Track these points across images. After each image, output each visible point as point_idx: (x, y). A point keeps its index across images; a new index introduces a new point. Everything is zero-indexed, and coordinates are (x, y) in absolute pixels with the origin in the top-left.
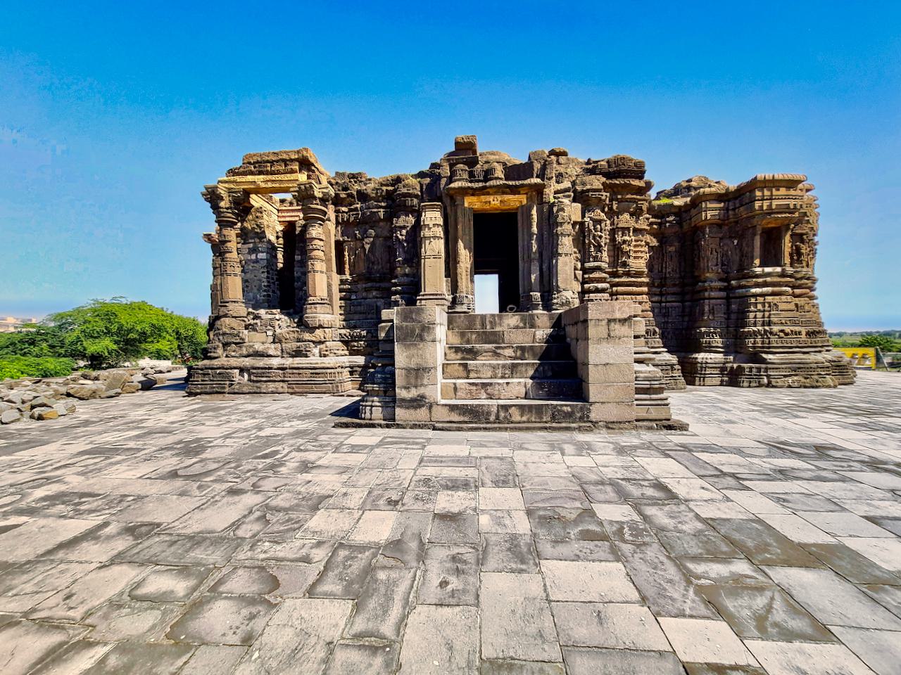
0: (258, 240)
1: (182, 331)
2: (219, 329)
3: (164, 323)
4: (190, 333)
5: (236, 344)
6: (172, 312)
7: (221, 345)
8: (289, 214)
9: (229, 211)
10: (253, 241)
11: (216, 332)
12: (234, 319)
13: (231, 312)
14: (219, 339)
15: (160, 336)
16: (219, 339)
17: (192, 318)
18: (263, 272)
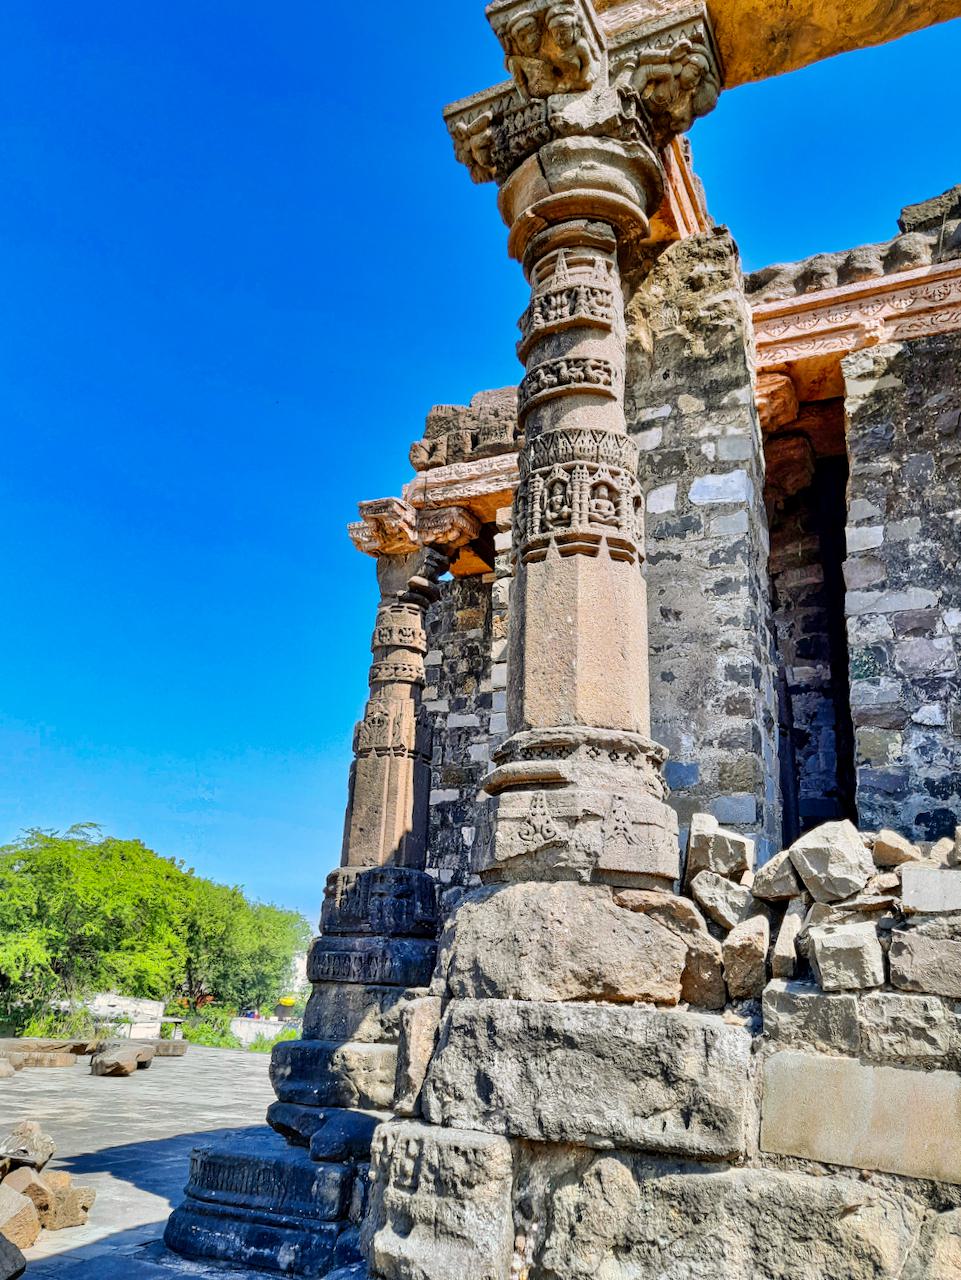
0: (699, 404)
1: (201, 922)
2: (488, 987)
3: (169, 899)
4: (221, 928)
5: (645, 1157)
6: (192, 870)
7: (500, 1153)
8: (823, 325)
9: (614, 146)
10: (666, 410)
11: (462, 1008)
12: (604, 897)
13: (588, 834)
14: (485, 1086)
15: (152, 932)
16: (485, 1086)
17: (231, 887)
18: (723, 587)
